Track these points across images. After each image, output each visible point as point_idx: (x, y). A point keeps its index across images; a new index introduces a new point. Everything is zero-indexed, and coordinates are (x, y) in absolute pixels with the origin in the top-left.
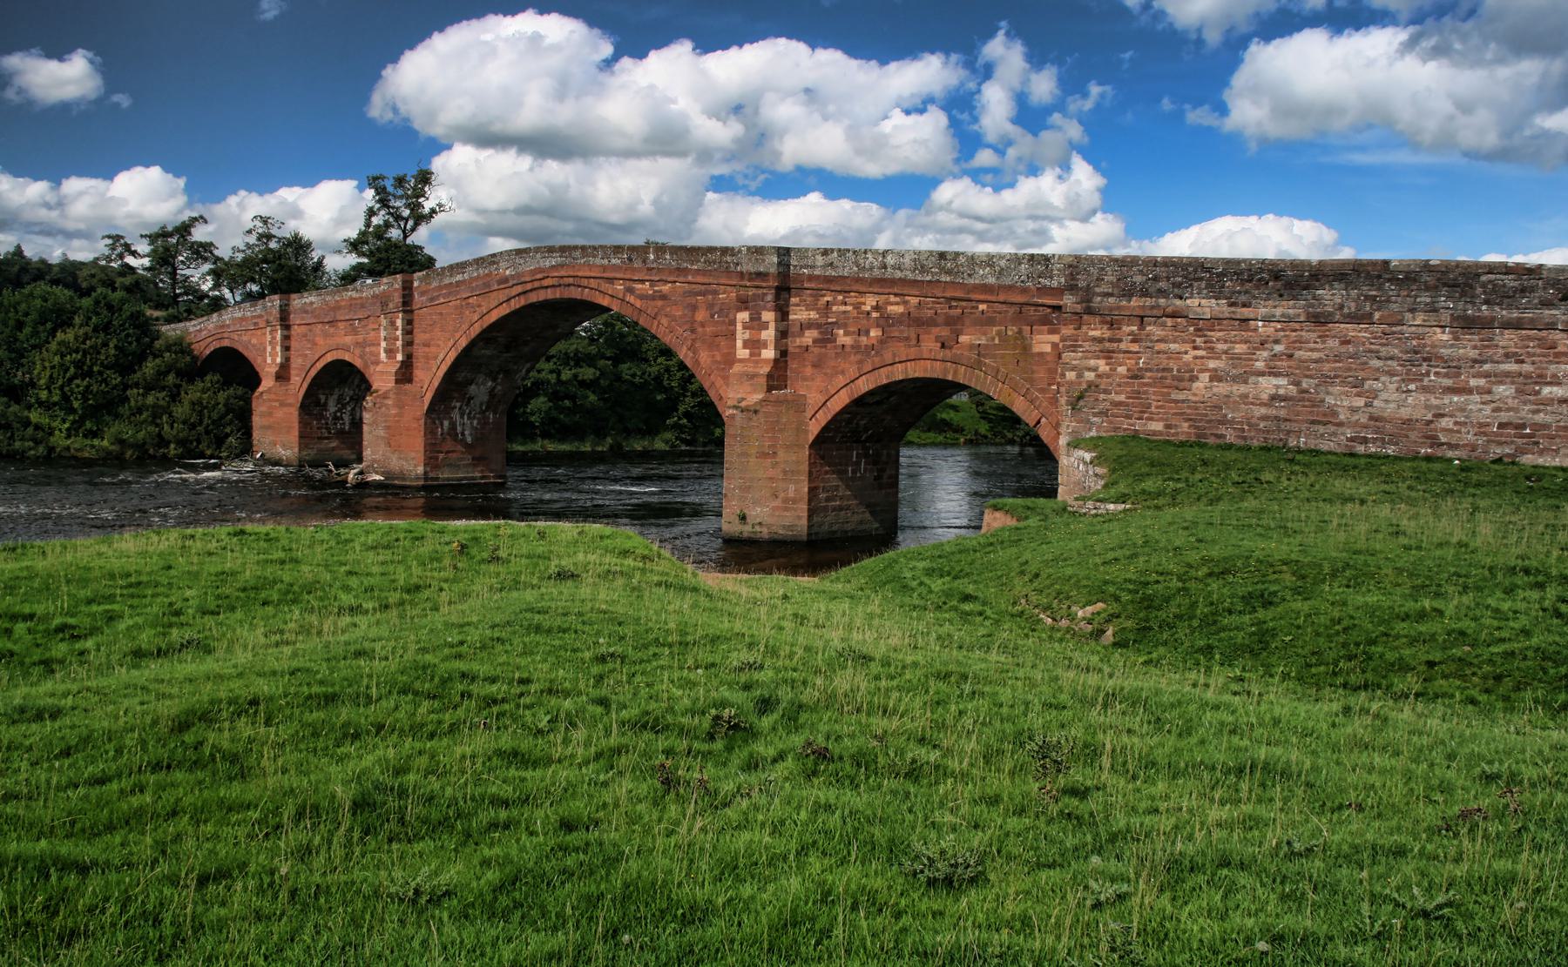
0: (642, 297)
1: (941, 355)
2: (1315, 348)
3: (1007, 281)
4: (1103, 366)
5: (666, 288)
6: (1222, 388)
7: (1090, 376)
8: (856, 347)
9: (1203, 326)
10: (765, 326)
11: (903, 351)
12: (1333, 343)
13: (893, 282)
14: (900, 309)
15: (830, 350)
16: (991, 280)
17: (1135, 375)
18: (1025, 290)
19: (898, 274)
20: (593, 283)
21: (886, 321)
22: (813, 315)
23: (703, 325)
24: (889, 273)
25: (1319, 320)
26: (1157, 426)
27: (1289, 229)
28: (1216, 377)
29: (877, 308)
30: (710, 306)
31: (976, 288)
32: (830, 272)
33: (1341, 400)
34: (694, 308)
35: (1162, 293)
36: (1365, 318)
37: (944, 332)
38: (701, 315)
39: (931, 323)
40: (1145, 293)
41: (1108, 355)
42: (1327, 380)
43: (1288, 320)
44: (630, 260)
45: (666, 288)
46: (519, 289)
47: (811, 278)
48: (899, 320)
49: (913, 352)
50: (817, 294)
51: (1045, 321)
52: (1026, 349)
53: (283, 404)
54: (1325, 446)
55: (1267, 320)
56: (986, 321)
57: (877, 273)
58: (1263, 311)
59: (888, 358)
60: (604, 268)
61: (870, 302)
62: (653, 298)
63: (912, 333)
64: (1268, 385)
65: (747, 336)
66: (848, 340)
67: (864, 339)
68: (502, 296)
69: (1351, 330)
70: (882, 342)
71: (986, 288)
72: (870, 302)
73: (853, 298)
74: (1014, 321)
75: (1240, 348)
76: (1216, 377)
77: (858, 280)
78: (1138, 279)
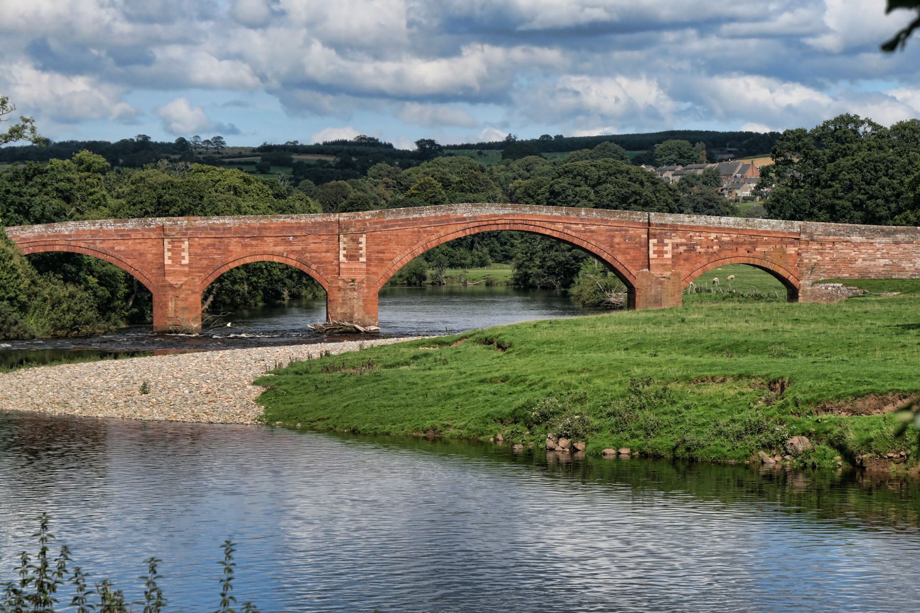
0: (576, 231)
1: (748, 255)
2: (895, 251)
3: (776, 230)
4: (819, 257)
5: (594, 228)
6: (867, 263)
7: (815, 261)
8: (707, 253)
9: (857, 245)
10: (170, 258)
11: (729, 254)
12: (901, 249)
13: (724, 229)
14: (728, 239)
15: (693, 254)
16: (769, 229)
17: (833, 260)
18: (783, 233)
19: (727, 226)
20: (538, 223)
21: (721, 243)
22: (683, 240)
23: (618, 244)
24: (722, 226)
25: (897, 243)
26: (847, 275)
27: (167, 123)
28: (864, 260)
29: (717, 238)
30: (624, 236)
31: (763, 232)
32: (692, 224)
33: (906, 265)
34: (613, 237)
35: (841, 235)
36: (912, 243)
37: (749, 247)
38: (617, 240)
39: (743, 243)
40: (835, 235)
41: (821, 254)
42: (901, 260)
43: (886, 243)
44: (567, 214)
45: (594, 228)
46: (476, 224)
47: (681, 226)
48: (727, 243)
49: (735, 254)
50: (685, 232)
51: (791, 243)
52: (784, 253)
53: (194, 292)
54: (904, 277)
55: (879, 243)
56: (767, 243)
57: (716, 225)
58: (878, 241)
59: (722, 256)
60: (549, 217)
61: (713, 236)
62: (585, 232)
63: (734, 247)
64: (882, 262)
65: (656, 248)
66: (702, 250)
67: (710, 250)
68: (459, 227)
69: (906, 246)
70: (719, 251)
71: (767, 232)
72: (713, 236)
73: (704, 234)
74: (779, 243)
75: (870, 251)
76: (864, 260)
77: (707, 228)
78: (832, 230)
